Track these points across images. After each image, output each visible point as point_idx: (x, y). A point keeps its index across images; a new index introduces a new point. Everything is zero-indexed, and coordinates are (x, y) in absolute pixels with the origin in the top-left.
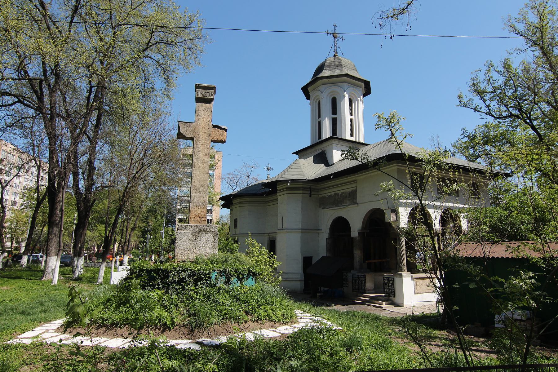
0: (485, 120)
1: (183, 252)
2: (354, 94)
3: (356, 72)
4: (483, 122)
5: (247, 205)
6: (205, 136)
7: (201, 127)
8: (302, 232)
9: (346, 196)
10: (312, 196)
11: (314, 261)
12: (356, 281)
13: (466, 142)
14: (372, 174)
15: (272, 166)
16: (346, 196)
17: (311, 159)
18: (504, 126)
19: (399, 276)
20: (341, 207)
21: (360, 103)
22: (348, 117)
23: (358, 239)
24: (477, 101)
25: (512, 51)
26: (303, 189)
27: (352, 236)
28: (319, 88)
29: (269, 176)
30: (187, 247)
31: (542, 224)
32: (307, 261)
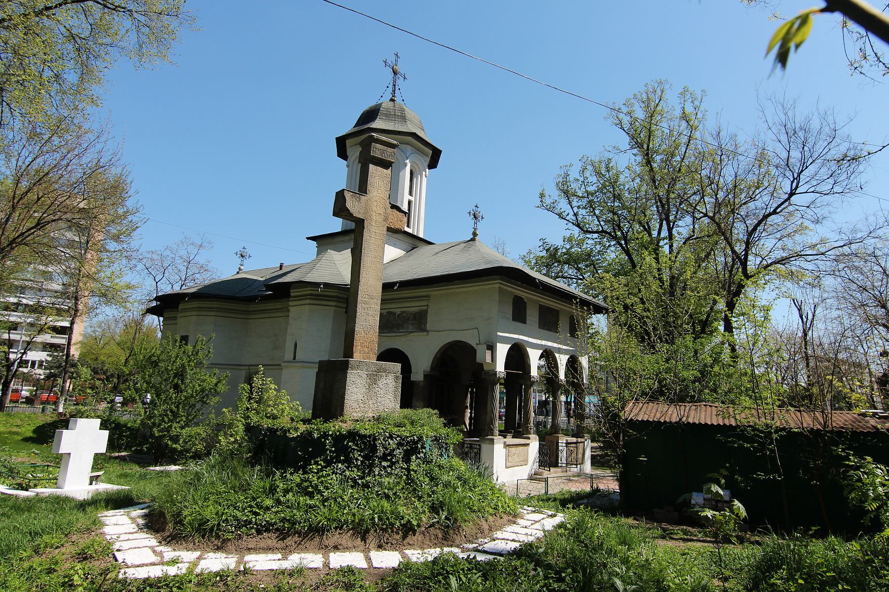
0: (571, 232)
1: (355, 405)
2: (417, 165)
3: (422, 132)
4: (567, 234)
6: (380, 219)
7: (375, 204)
9: (408, 318)
13: (542, 257)
14: (457, 290)
15: (249, 251)
16: (408, 318)
18: (590, 243)
19: (488, 442)
20: (394, 334)
21: (424, 179)
23: (422, 384)
24: (563, 205)
26: (338, 299)
27: (412, 379)
29: (242, 267)
30: (361, 397)
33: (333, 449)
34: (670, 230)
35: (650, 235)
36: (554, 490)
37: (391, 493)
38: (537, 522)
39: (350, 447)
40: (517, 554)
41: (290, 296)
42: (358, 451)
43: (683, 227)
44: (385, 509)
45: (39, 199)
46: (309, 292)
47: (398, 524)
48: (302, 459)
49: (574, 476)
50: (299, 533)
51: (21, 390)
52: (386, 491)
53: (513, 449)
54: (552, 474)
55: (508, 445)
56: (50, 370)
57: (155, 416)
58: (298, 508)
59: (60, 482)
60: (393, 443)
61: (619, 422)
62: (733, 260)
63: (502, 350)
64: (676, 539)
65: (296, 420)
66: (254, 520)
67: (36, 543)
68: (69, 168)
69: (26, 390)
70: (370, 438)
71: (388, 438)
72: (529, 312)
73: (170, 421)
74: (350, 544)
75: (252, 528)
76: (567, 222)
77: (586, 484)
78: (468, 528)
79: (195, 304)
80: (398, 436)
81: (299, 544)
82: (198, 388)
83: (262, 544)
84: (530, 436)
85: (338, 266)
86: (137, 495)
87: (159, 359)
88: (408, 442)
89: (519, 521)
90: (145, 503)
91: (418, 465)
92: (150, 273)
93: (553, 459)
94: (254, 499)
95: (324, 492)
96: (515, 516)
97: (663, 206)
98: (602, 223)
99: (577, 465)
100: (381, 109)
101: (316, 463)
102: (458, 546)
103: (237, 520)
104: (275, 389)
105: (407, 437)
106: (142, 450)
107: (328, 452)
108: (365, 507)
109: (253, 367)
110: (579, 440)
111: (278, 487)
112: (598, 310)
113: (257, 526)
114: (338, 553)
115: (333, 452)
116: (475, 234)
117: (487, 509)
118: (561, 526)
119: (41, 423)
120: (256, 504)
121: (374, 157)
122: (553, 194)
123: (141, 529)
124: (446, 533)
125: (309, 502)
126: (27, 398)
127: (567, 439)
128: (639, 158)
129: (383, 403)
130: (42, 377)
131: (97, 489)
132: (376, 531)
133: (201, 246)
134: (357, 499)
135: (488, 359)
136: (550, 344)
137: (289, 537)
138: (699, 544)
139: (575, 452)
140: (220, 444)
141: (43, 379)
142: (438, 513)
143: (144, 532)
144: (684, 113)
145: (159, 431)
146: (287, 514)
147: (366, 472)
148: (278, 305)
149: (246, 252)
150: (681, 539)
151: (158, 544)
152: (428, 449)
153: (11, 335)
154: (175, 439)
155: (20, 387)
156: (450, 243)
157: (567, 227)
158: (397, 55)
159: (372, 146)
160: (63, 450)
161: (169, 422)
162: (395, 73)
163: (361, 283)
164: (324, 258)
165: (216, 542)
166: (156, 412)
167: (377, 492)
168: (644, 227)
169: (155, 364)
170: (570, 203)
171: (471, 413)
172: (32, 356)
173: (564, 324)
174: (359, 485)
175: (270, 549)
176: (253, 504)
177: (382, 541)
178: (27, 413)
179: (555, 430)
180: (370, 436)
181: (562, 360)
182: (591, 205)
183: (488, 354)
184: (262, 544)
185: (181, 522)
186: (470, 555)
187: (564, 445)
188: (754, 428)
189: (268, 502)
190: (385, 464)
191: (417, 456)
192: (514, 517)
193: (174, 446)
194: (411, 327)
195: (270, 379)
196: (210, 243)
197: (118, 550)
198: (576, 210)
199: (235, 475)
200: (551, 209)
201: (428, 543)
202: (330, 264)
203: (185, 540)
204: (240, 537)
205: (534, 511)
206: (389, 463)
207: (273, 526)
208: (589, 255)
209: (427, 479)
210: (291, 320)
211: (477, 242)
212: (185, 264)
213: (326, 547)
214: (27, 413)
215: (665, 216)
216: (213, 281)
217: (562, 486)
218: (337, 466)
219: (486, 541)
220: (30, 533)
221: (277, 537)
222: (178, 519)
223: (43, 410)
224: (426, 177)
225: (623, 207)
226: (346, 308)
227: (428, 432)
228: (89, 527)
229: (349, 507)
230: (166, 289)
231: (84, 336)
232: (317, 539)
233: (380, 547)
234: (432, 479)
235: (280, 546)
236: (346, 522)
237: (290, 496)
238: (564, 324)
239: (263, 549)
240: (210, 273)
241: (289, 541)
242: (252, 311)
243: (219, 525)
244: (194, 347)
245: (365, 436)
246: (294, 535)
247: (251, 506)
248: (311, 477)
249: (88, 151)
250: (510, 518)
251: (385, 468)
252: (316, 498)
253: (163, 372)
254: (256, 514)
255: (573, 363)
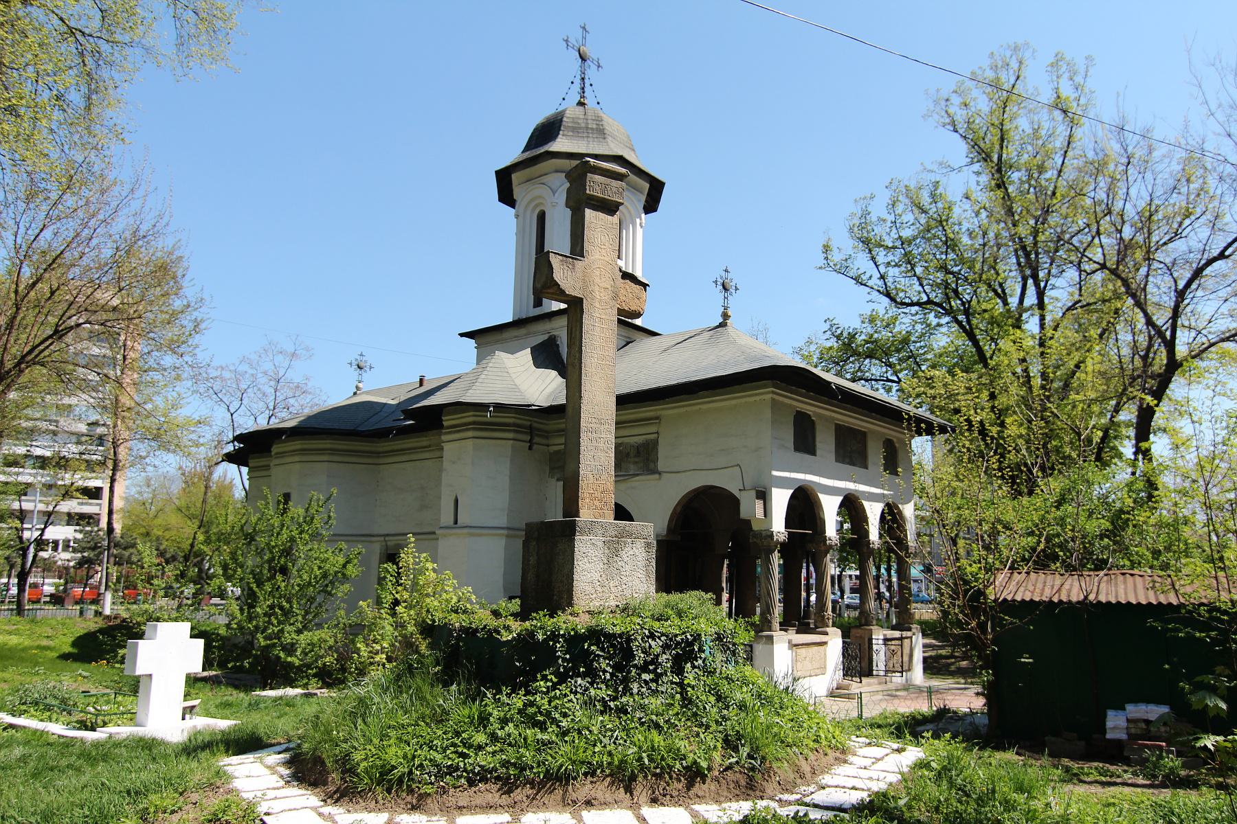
1: (589, 589)
2: (629, 212)
3: (632, 153)
5: (325, 458)
7: (598, 273)
8: (508, 536)
10: (535, 447)
14: (704, 407)
15: (369, 359)
17: (526, 355)
18: (906, 322)
21: (640, 231)
24: (862, 263)
25: (934, 167)
26: (517, 428)
28: (544, 179)
29: (360, 385)
30: (596, 576)
33: (568, 656)
34: (1041, 294)
35: (1005, 303)
36: (870, 712)
37: (661, 722)
38: (879, 760)
39: (593, 652)
40: (861, 809)
41: (442, 426)
42: (605, 658)
43: (1061, 290)
44: (656, 745)
45: (53, 293)
46: (471, 419)
47: (678, 766)
48: (521, 672)
49: (897, 690)
50: (532, 783)
51: (43, 584)
52: (654, 717)
53: (803, 651)
54: (866, 687)
55: (796, 645)
56: (81, 552)
57: (257, 616)
58: (526, 746)
59: (140, 716)
60: (656, 646)
61: (985, 603)
62: (1151, 338)
63: (780, 499)
64: (1090, 783)
65: (504, 614)
66: (462, 765)
67: (141, 806)
68: (94, 242)
69: (49, 584)
70: (621, 638)
71: (648, 637)
72: (820, 437)
73: (279, 623)
74: (609, 797)
75: (461, 776)
76: (868, 290)
77: (920, 701)
78: (783, 770)
79: (297, 444)
80: (663, 634)
81: (533, 799)
82: (318, 573)
83: (479, 800)
84: (828, 629)
85: (514, 376)
86: (266, 733)
87: (255, 529)
88: (678, 643)
89: (851, 758)
90: (280, 744)
91: (697, 678)
92: (221, 400)
93: (865, 664)
94: (458, 734)
95: (561, 721)
96: (843, 752)
97: (1027, 255)
98: (927, 288)
99: (902, 672)
100: (565, 119)
101: (544, 678)
102: (772, 799)
103: (437, 766)
104: (434, 570)
105: (676, 636)
106: (242, 666)
107: (560, 661)
108: (625, 741)
109: (391, 538)
110: (905, 634)
111: (490, 714)
112: (928, 429)
113: (468, 774)
114: (593, 812)
115: (568, 661)
116: (725, 316)
117: (806, 741)
118: (922, 765)
119: (82, 632)
120: (461, 742)
121: (591, 198)
122: (845, 245)
123: (289, 782)
124: (751, 779)
125: (539, 736)
126: (52, 596)
127: (885, 632)
128: (985, 179)
129: (630, 584)
130: (72, 564)
131: (195, 727)
132: (645, 777)
133: (294, 354)
134: (613, 731)
135: (759, 513)
136: (851, 486)
137: (517, 788)
138: (1127, 790)
139: (899, 653)
140: (358, 654)
141: (74, 567)
142: (736, 749)
143: (294, 786)
144: (1059, 97)
145: (266, 638)
146: (510, 754)
147: (620, 689)
148: (424, 441)
149: (366, 362)
150: (1096, 782)
151: (322, 803)
152: (707, 652)
153: (23, 503)
154: (290, 649)
155: (40, 581)
156: (680, 334)
157: (869, 297)
158: (584, 28)
159: (588, 179)
160: (140, 670)
161: (279, 625)
162: (583, 58)
163: (584, 401)
164: (491, 365)
165: (409, 798)
166: (258, 610)
167: (640, 719)
168: (995, 291)
169: (250, 538)
170: (873, 259)
171: (730, 601)
172: (53, 533)
173: (876, 456)
174: (612, 709)
175: (491, 807)
176: (457, 741)
177: (657, 792)
178: (59, 619)
179: (866, 620)
180: (621, 636)
181: (873, 511)
182: (909, 260)
183: (759, 505)
184: (479, 800)
185: (352, 771)
186: (798, 811)
187: (881, 642)
188: (1212, 608)
189: (481, 738)
190: (645, 676)
191: (692, 663)
192: (843, 754)
193: (289, 659)
194: (632, 466)
195: (425, 555)
196: (307, 349)
197: (267, 814)
198: (882, 269)
199: (422, 699)
200: (842, 270)
201: (725, 793)
202: (500, 374)
203: (361, 797)
204: (444, 791)
205: (870, 743)
206: (652, 676)
207: (491, 772)
208: (906, 341)
209: (712, 699)
210: (446, 464)
211: (729, 329)
212: (273, 383)
213: (574, 802)
214: (59, 619)
215: (1030, 271)
216: (316, 410)
217: (884, 705)
218: (576, 682)
219: (811, 789)
220: (129, 793)
221: (499, 790)
222: (346, 766)
223: (81, 613)
224: (641, 227)
225: (962, 261)
226: (530, 441)
227: (706, 629)
228: (212, 781)
229: (601, 743)
230: (248, 425)
231: (126, 499)
232: (559, 792)
233: (654, 801)
234: (719, 698)
235: (505, 803)
236: (600, 765)
237: (510, 728)
238: (876, 456)
239: (481, 807)
240: (310, 397)
241: (519, 794)
242: (383, 452)
243: (410, 773)
244: (307, 510)
245: (614, 636)
246: (525, 785)
247: (454, 745)
248: (538, 699)
249: (120, 213)
250: (838, 754)
251: (646, 682)
252: (550, 730)
253: (263, 549)
254: (464, 756)
255: (892, 518)
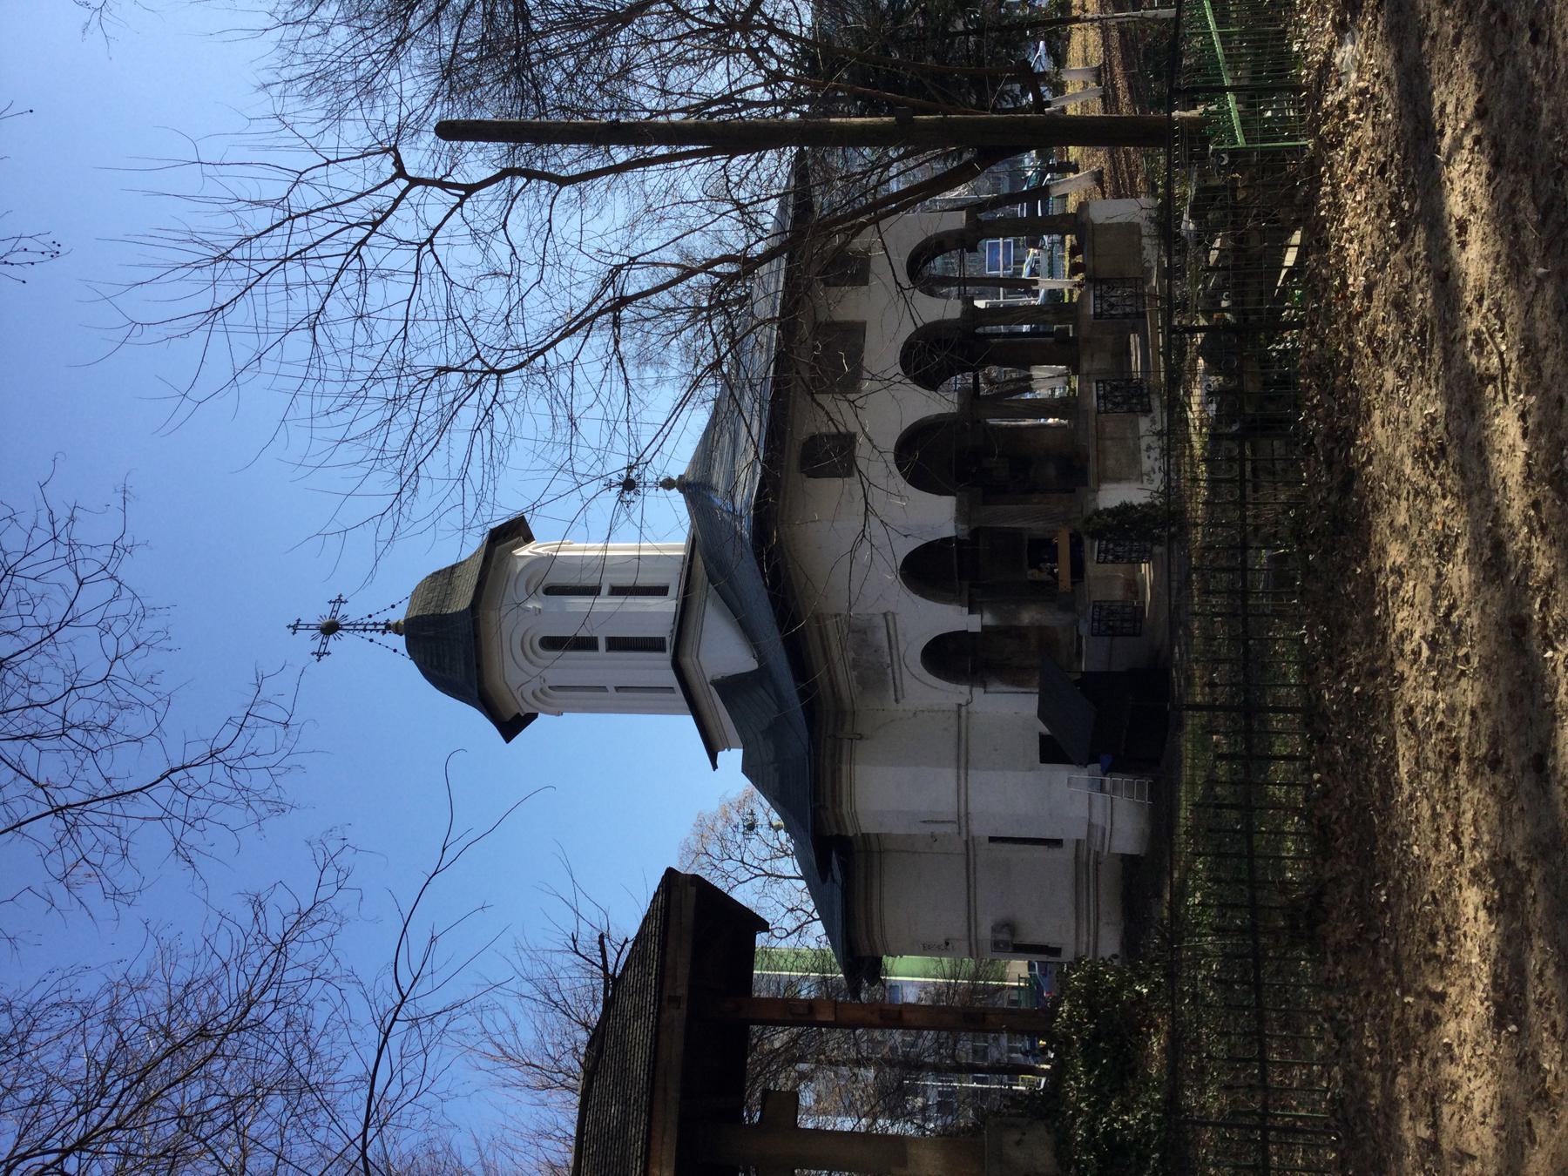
11: (1045, 730)
12: (1110, 628)
22: (605, 603)
31: (1307, 57)
32: (1051, 752)
